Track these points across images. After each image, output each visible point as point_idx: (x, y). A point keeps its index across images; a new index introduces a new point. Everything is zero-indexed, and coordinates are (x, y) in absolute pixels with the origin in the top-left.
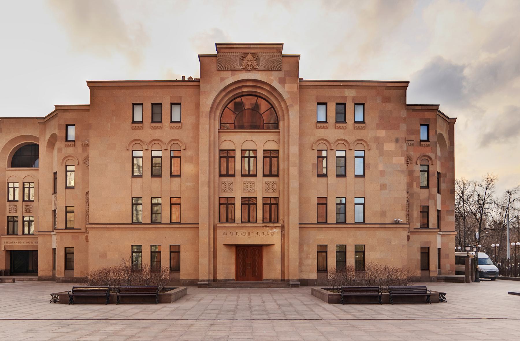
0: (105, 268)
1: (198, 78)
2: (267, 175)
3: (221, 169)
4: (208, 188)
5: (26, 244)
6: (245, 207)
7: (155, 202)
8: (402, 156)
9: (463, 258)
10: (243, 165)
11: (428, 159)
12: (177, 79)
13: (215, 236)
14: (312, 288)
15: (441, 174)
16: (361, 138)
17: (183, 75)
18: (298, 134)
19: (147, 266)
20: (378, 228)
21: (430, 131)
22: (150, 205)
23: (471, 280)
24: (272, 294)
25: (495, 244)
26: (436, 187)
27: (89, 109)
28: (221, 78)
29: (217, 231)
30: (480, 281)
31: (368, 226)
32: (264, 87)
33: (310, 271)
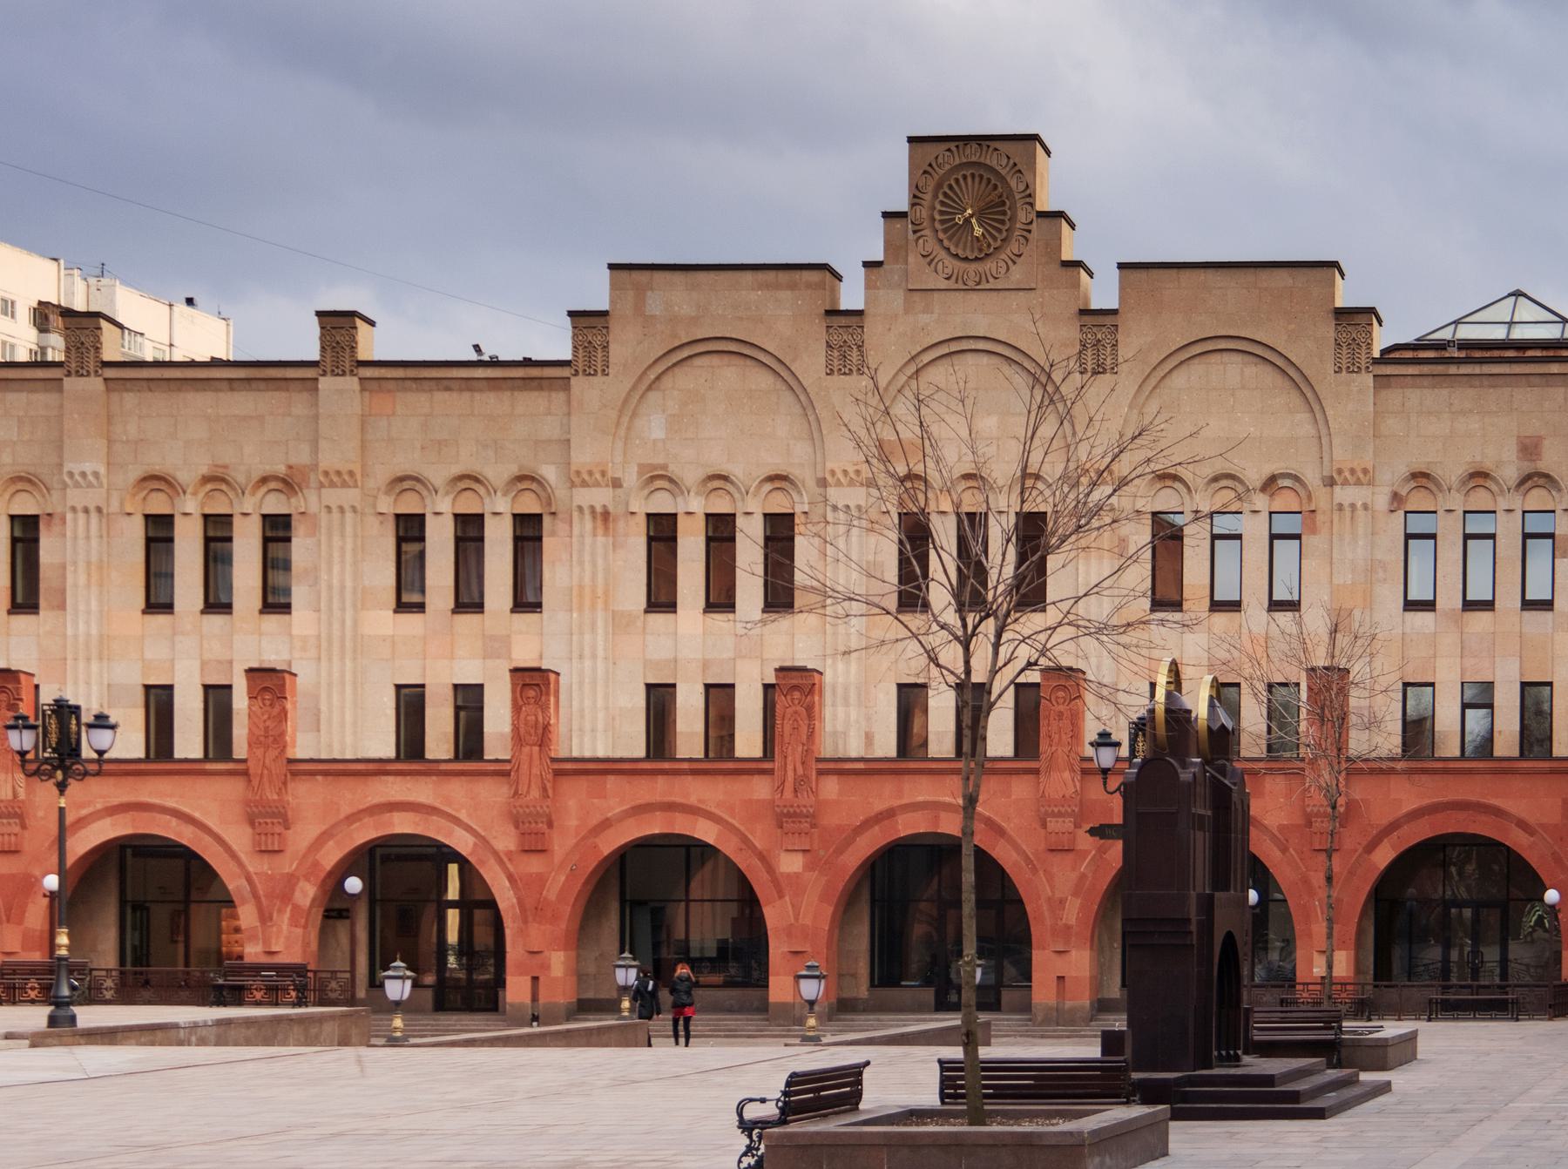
4: (691, 939)
5: (288, 914)
8: (521, 974)
10: (797, 275)
11: (1480, 481)
12: (477, 348)
22: (1520, 538)
27: (1061, 978)
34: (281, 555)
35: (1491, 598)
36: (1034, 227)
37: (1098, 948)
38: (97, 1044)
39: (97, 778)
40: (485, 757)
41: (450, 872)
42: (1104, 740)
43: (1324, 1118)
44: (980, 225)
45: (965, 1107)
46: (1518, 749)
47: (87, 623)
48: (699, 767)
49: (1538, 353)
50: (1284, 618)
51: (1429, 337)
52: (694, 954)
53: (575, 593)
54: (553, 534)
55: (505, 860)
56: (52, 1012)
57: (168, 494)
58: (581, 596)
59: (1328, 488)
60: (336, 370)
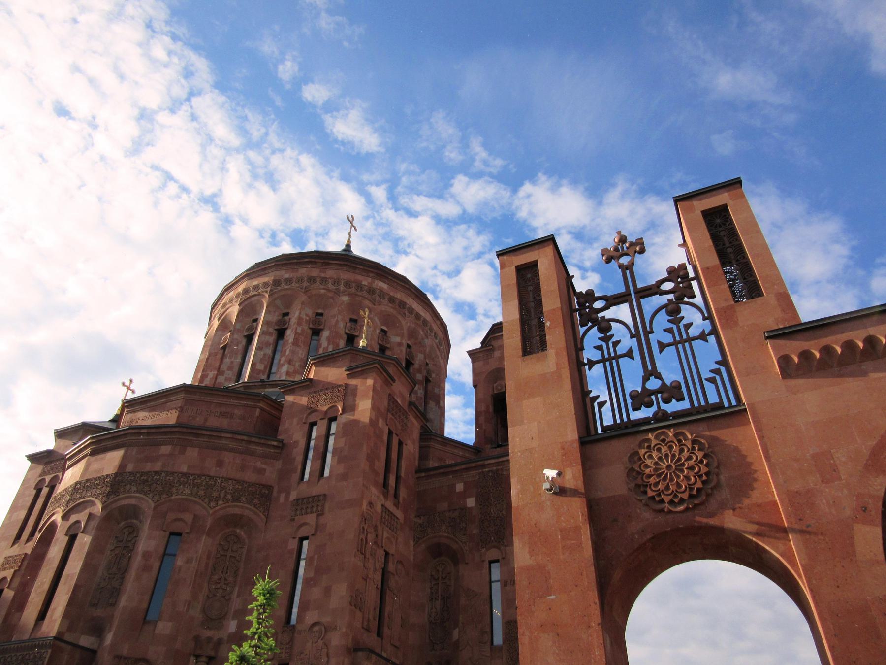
0: (233, 226)
1: (407, 277)
2: (735, 406)
3: (562, 267)
6: (194, 118)
7: (467, 423)
9: (304, 400)
12: (131, 381)
14: (577, 529)
16: (313, 622)
18: (562, 324)
19: (493, 511)
20: (179, 391)
21: (488, 593)
23: (506, 458)
30: (666, 275)
31: (81, 455)
32: (223, 435)
33: (309, 414)
36: (333, 627)
38: (38, 615)
39: (304, 497)
40: (718, 401)
41: (330, 439)
43: (845, 342)
44: (508, 238)
49: (243, 396)
50: (320, 311)
53: (321, 638)
54: (324, 246)
55: (248, 296)
56: (666, 310)
58: (746, 265)
59: (388, 334)
60: (564, 462)
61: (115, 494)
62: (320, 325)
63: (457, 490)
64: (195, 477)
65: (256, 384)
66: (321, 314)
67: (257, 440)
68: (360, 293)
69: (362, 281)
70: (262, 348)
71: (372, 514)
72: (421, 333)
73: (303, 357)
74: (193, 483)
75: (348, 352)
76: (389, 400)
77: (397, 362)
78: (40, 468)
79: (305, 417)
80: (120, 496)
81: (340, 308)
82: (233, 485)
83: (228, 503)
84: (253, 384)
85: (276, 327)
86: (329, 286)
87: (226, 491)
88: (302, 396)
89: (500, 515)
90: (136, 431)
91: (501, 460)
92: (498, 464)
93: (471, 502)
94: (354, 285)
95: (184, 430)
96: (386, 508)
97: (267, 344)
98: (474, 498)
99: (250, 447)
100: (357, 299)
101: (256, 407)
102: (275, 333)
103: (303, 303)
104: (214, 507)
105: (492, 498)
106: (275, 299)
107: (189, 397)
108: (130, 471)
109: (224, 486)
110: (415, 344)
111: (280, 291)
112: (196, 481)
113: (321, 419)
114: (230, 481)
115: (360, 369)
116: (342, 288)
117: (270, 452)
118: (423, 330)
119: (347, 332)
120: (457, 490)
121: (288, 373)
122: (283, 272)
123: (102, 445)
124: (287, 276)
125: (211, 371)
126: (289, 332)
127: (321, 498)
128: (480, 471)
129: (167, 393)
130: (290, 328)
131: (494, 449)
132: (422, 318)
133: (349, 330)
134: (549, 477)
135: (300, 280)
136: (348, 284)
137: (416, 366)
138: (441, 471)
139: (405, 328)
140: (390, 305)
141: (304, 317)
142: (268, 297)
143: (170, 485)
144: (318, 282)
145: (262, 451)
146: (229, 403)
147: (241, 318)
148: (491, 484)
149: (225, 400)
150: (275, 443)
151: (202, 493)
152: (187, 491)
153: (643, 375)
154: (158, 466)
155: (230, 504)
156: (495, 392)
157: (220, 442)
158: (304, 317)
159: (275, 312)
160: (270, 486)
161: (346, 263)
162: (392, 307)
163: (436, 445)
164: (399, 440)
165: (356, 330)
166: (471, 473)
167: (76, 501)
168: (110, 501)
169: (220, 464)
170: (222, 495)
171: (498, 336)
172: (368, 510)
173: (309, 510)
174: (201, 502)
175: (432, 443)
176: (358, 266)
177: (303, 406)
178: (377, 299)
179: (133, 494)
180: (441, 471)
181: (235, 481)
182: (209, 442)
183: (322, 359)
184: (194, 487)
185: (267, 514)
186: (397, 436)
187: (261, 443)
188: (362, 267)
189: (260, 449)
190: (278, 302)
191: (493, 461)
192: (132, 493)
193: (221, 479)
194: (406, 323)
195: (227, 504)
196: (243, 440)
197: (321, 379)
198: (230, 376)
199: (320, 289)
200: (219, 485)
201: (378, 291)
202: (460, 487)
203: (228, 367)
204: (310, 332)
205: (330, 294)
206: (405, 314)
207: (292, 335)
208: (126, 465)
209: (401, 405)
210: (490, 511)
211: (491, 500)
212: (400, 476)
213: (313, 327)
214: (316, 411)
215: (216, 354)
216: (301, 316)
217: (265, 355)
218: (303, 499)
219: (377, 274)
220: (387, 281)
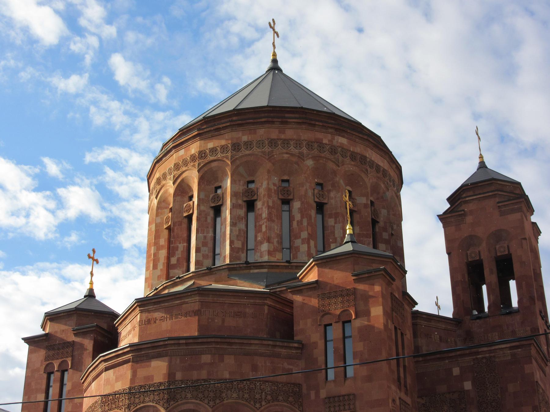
10: (246, 234)
12: (94, 251)
13: (192, 337)
15: (319, 279)
17: (156, 270)
19: (490, 394)
24: (423, 397)
25: (27, 223)
26: (212, 252)
28: (163, 202)
29: (294, 337)
33: (323, 316)
34: (549, 325)
35: (396, 360)
37: (186, 263)
42: (101, 410)
45: (298, 275)
46: (323, 249)
47: (208, 352)
48: (190, 137)
50: (286, 178)
51: (191, 288)
52: (301, 345)
55: (206, 161)
57: (265, 74)
61: (174, 401)
62: (289, 195)
63: (454, 374)
64: (238, 382)
65: (241, 266)
66: (287, 181)
67: (281, 344)
68: (323, 155)
69: (322, 140)
70: (236, 223)
71: (395, 409)
72: (383, 186)
73: (278, 232)
74: (238, 388)
75: (350, 256)
76: (392, 299)
77: (393, 260)
78: (42, 353)
79: (319, 319)
80: (180, 402)
81: (306, 175)
82: (270, 387)
83: (269, 403)
84: (238, 266)
85: (245, 199)
86: (292, 150)
87: (265, 393)
88: (310, 297)
89: (496, 398)
90: (176, 342)
91: (493, 348)
92: (490, 352)
93: (468, 385)
94: (316, 146)
95: (219, 340)
96: (402, 400)
97: (240, 218)
98: (470, 382)
99: (276, 350)
100: (321, 161)
101: (264, 304)
102: (244, 204)
103: (269, 172)
104: (260, 408)
105: (487, 383)
106: (238, 167)
107: (204, 299)
108: (180, 379)
109: (263, 388)
110: (378, 199)
111: (241, 157)
112: (239, 386)
113: (336, 322)
114: (267, 383)
115: (367, 275)
116: (305, 150)
117: (293, 353)
118: (384, 183)
119: (317, 200)
120: (454, 374)
121: (270, 253)
122: (240, 134)
123: (143, 353)
124: (245, 138)
125: (180, 243)
126: (259, 205)
127: (351, 397)
128: (474, 357)
129: (182, 295)
130: (260, 200)
131: (474, 321)
132: (382, 169)
133: (318, 198)
134: (83, 355)
135: (260, 144)
136: (310, 145)
137: (381, 224)
138: (438, 356)
139: (369, 185)
140: (353, 163)
141: (272, 187)
142: (230, 163)
143: (220, 391)
144: (280, 146)
145: (286, 353)
146: (239, 303)
147: (203, 186)
148: (485, 370)
149: (236, 300)
150: (296, 345)
151: (246, 396)
152: (235, 395)
153: (512, 280)
154: (204, 374)
155: (271, 404)
156: (470, 260)
157: (250, 348)
158: (272, 187)
159: (240, 181)
160: (299, 384)
161: (305, 121)
162: (354, 165)
163: (422, 322)
164: (401, 332)
165: (324, 197)
166: (466, 358)
167: (137, 406)
168: (171, 407)
169: (255, 368)
170: (263, 397)
171: (468, 200)
172: (393, 407)
173: (342, 408)
174: (248, 404)
175: (419, 321)
176: (317, 123)
177: (313, 307)
178: (341, 159)
179: (190, 401)
180: (438, 356)
181: (271, 382)
182: (241, 349)
183: (324, 261)
184: (239, 391)
185: (301, 409)
186: (400, 329)
187: (284, 346)
188: (321, 124)
189: (284, 351)
190: (241, 170)
191: (485, 349)
192: (188, 399)
193: (259, 383)
194: (369, 180)
195: (268, 405)
196: (269, 345)
197: (325, 280)
198: (207, 253)
199: (283, 153)
200: (259, 388)
201: (339, 149)
202: (456, 371)
203: (203, 242)
204: (279, 202)
205: (294, 159)
206: (367, 170)
207: (264, 209)
208: (174, 375)
209: (398, 297)
210: (487, 395)
211: (487, 385)
212: (405, 365)
213: (283, 197)
214: (329, 314)
215: (180, 223)
216: (270, 186)
217: (240, 230)
218: (334, 397)
219: (336, 130)
220: (346, 136)
